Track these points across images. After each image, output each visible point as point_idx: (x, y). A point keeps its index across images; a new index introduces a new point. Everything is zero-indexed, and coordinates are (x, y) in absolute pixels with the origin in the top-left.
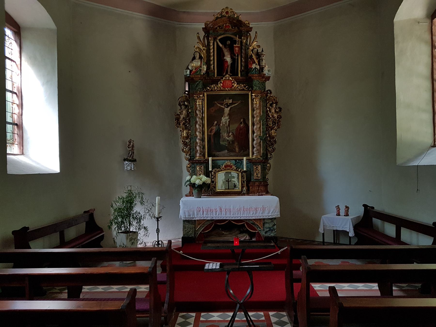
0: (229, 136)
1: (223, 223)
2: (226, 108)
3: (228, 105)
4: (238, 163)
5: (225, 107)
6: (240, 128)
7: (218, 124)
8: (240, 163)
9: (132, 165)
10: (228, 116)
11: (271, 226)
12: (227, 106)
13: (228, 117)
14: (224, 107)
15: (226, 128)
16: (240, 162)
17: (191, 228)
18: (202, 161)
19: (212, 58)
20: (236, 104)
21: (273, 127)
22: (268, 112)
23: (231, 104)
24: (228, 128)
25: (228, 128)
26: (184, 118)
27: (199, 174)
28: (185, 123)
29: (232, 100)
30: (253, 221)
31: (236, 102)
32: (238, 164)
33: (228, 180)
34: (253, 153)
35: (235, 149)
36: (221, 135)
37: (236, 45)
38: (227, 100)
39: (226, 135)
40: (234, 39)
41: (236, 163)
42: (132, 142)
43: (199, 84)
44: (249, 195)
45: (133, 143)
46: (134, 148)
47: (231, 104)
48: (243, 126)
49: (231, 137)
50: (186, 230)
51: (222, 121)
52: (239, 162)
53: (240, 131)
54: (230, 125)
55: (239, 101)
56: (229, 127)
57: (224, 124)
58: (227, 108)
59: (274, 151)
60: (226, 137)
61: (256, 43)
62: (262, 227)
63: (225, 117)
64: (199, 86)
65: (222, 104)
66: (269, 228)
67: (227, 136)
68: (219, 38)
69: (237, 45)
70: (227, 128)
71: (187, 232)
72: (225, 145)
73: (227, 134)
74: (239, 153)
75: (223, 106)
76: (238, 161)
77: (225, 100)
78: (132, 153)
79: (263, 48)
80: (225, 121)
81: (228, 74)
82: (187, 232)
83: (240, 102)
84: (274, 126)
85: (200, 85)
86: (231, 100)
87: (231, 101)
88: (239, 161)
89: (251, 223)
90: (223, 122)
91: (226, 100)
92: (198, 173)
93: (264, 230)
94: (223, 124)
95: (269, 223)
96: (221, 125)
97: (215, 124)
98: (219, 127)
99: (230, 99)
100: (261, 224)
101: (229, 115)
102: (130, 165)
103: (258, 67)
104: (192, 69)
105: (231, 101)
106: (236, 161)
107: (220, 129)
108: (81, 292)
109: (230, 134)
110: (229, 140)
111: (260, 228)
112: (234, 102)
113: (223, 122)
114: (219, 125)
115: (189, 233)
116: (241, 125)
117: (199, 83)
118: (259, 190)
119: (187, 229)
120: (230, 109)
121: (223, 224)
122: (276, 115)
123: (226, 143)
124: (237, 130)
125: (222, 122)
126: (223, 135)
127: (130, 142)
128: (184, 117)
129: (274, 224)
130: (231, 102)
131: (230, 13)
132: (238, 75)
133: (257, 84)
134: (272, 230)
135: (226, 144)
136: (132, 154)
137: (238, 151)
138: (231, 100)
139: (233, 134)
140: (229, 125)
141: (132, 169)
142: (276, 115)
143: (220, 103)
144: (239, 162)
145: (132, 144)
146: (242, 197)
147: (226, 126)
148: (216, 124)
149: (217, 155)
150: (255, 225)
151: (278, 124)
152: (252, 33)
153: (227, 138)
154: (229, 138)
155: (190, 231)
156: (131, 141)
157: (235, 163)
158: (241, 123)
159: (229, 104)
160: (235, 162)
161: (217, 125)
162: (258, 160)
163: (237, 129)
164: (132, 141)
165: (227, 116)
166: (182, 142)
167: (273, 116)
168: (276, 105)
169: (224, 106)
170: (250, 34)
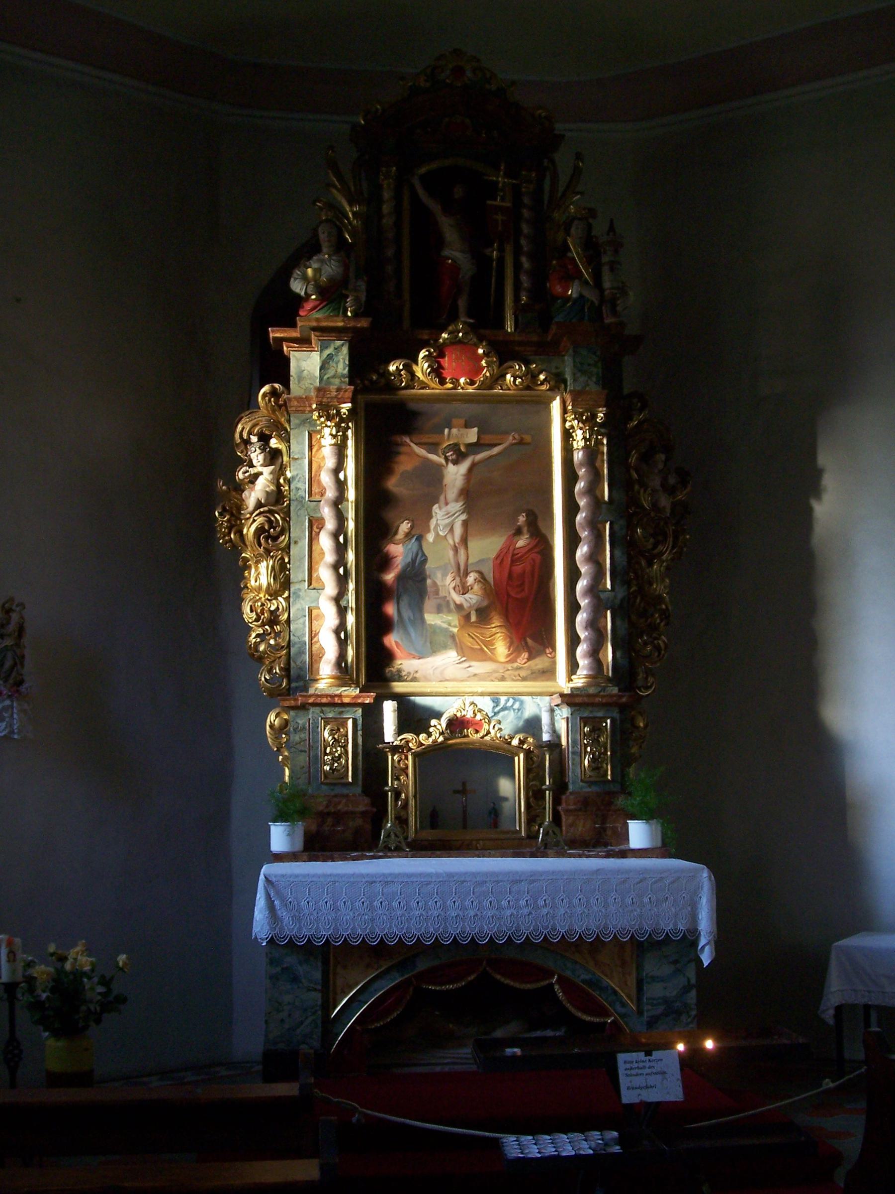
0: (464, 590)
1: (449, 984)
2: (451, 466)
3: (460, 449)
4: (504, 709)
5: (446, 459)
6: (513, 555)
7: (413, 533)
8: (514, 710)
9: (15, 716)
10: (462, 497)
11: (675, 993)
12: (454, 457)
13: (461, 503)
14: (443, 462)
15: (451, 553)
16: (517, 706)
17: (305, 1010)
18: (347, 696)
19: (390, 252)
20: (496, 450)
21: (655, 552)
22: (637, 487)
23: (475, 448)
24: (462, 552)
25: (462, 552)
26: (259, 505)
27: (332, 759)
28: (266, 527)
29: (479, 433)
30: (594, 974)
31: (495, 442)
32: (506, 712)
33: (461, 788)
34: (573, 666)
35: (493, 645)
36: (429, 581)
37: (495, 200)
38: (454, 431)
39: (453, 585)
40: (486, 178)
41: (497, 710)
42: (18, 609)
43: (336, 359)
44: (563, 856)
45: (22, 617)
46: (26, 640)
47: (475, 448)
48: (528, 544)
49: (473, 593)
50: (282, 1021)
51: (433, 523)
52: (509, 704)
53: (514, 568)
54: (469, 538)
55: (511, 438)
56: (466, 548)
57: (441, 533)
58: (456, 462)
59: (660, 660)
60: (452, 591)
61: (579, 196)
62: (635, 999)
63: (447, 504)
64: (337, 363)
65: (433, 447)
66: (666, 1001)
67: (454, 588)
68: (423, 170)
69: (498, 202)
70: (456, 550)
71: (289, 1029)
72: (445, 625)
73: (458, 579)
74: (509, 666)
75: (440, 457)
76: (507, 701)
77: (446, 431)
78: (14, 658)
79: (612, 221)
80: (447, 521)
81: (463, 319)
82: (287, 1026)
83: (514, 438)
84: (660, 548)
85: (339, 361)
86: (476, 429)
87: (472, 435)
88: (511, 701)
89: (584, 981)
90: (437, 525)
91: (450, 429)
92: (326, 754)
93: (640, 1012)
94: (437, 535)
95: (662, 981)
96: (430, 537)
97: (400, 535)
98: (420, 547)
99: (467, 425)
100: (628, 983)
101: (468, 495)
102: (6, 715)
103: (591, 295)
104: (306, 293)
105: (472, 435)
106: (496, 702)
107: (424, 554)
108: (577, 1157)
109: (471, 579)
110: (466, 605)
111: (623, 1005)
112: (487, 439)
113: (437, 525)
114: (420, 538)
115: (298, 1031)
116: (516, 538)
117: (337, 355)
118: (605, 830)
119: (290, 1015)
120: (470, 470)
121: (448, 991)
122: (665, 502)
123: (450, 618)
124: (502, 561)
125: (432, 527)
126: (439, 583)
127: (8, 611)
128: (263, 501)
129: (686, 984)
130: (475, 440)
131: (469, 74)
132: (501, 325)
133: (589, 365)
134: (679, 1013)
135: (450, 625)
136: (15, 664)
137: (508, 656)
138: (476, 429)
139: (482, 578)
140: (464, 540)
141: (16, 737)
142: (665, 502)
143: (425, 444)
144: (509, 704)
145: (15, 617)
146: (369, 862)
147: (451, 542)
148: (408, 535)
149: (409, 673)
150: (604, 989)
151: (676, 538)
152: (563, 160)
153: (458, 598)
154: (466, 596)
155: (302, 1023)
156: (14, 607)
157: (494, 707)
158: (518, 532)
159: (463, 449)
160: (492, 704)
161: (411, 539)
162: (603, 697)
163: (500, 559)
164: (17, 606)
165: (457, 501)
166: (252, 611)
167: (655, 506)
168: (667, 460)
169: (444, 453)
170: (553, 162)
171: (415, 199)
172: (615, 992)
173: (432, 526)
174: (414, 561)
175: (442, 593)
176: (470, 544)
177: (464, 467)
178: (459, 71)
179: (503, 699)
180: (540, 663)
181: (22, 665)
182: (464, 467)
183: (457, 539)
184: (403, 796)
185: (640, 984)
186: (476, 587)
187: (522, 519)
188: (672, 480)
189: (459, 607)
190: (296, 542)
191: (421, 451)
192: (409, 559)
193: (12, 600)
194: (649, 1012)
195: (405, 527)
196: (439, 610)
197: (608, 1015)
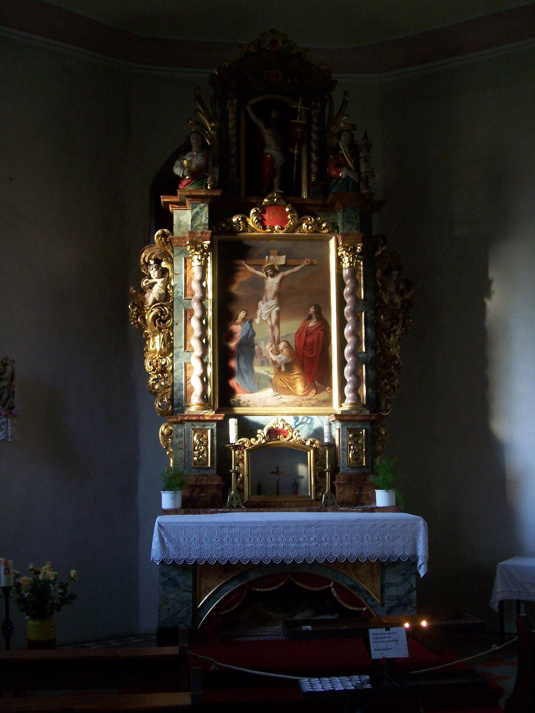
0: (277, 352)
1: (269, 587)
2: (269, 278)
3: (275, 268)
4: (302, 423)
5: (267, 274)
6: (307, 331)
7: (247, 318)
8: (307, 424)
9: (9, 428)
10: (276, 297)
11: (403, 593)
12: (271, 273)
13: (276, 301)
14: (265, 276)
15: (270, 330)
16: (309, 421)
17: (183, 603)
18: (208, 416)
19: (233, 151)
20: (296, 269)
21: (392, 329)
22: (380, 291)
23: (284, 267)
24: (276, 329)
25: (276, 329)
26: (155, 301)
27: (199, 453)
28: (159, 315)
29: (286, 258)
30: (355, 581)
31: (296, 264)
32: (303, 425)
33: (275, 471)
34: (342, 398)
35: (295, 385)
36: (256, 347)
37: (296, 119)
38: (272, 257)
39: (271, 349)
40: (290, 106)
41: (297, 424)
42: (11, 364)
43: (201, 214)
44: (337, 511)
45: (13, 369)
46: (16, 382)
47: (284, 267)
48: (316, 325)
49: (283, 354)
50: (169, 609)
51: (259, 312)
52: (305, 420)
53: (307, 339)
54: (280, 322)
55: (305, 261)
56: (279, 327)
57: (264, 318)
58: (272, 276)
59: (394, 394)
60: (270, 353)
61: (346, 117)
62: (379, 596)
63: (267, 301)
64: (201, 217)
65: (259, 267)
66: (398, 598)
67: (272, 351)
68: (253, 102)
69: (298, 121)
70: (272, 328)
71: (173, 615)
72: (266, 374)
73: (274, 346)
74: (304, 398)
75: (263, 273)
76: (303, 418)
77: (267, 257)
78: (8, 393)
79: (366, 132)
80: (267, 311)
81: (277, 191)
82: (172, 613)
83: (307, 262)
84: (395, 327)
85: (203, 216)
86: (284, 256)
87: (282, 260)
88: (306, 419)
89: (349, 586)
90: (261, 313)
91: (269, 256)
92: (195, 450)
93: (383, 605)
94: (261, 319)
95: (396, 586)
96: (257, 321)
97: (239, 320)
98: (251, 327)
99: (279, 254)
100: (376, 587)
101: (280, 295)
102: (3, 427)
103: (353, 176)
104: (183, 175)
105: (282, 260)
106: (297, 419)
107: (253, 331)
108: (345, 691)
109: (281, 346)
110: (278, 361)
111: (373, 600)
112: (291, 262)
113: (261, 313)
114: (251, 322)
115: (178, 616)
116: (309, 321)
117: (201, 212)
118: (361, 495)
119: (173, 606)
120: (281, 281)
121: (268, 592)
122: (397, 300)
123: (269, 369)
124: (300, 335)
125: (258, 315)
126: (262, 348)
127: (5, 365)
128: (157, 299)
129: (410, 587)
130: (284, 263)
131: (280, 44)
132: (300, 194)
133: (352, 218)
134: (406, 605)
135: (269, 373)
136: (9, 397)
137: (304, 391)
138: (284, 256)
139: (288, 345)
140: (278, 323)
141: (9, 440)
142: (397, 300)
143: (254, 265)
144: (305, 420)
145: (9, 368)
146: (221, 515)
147: (270, 324)
148: (244, 320)
149: (245, 402)
150: (361, 591)
151: (404, 321)
152: (337, 95)
153: (274, 357)
154: (279, 356)
155: (180, 611)
156: (8, 363)
157: (295, 422)
158: (310, 318)
159: (277, 268)
160: (294, 421)
161: (245, 322)
162: (360, 416)
163: (299, 334)
164: (10, 362)
165: (273, 299)
166: (150, 365)
167: (391, 302)
168: (399, 274)
169: (265, 271)
170: (330, 96)
171: (248, 119)
172: (368, 593)
173: (258, 314)
174: (247, 335)
175: (264, 354)
176: (281, 325)
177: (277, 279)
178: (274, 43)
179: (301, 418)
180: (323, 396)
181: (13, 397)
182: (277, 279)
183: (273, 322)
184: (241, 475)
185: (382, 587)
186: (285, 351)
187: (312, 310)
188: (402, 287)
189: (275, 363)
190: (177, 324)
191: (252, 270)
192: (245, 334)
193: (7, 358)
194: (388, 604)
195: (242, 315)
196: (262, 364)
197: (364, 606)
